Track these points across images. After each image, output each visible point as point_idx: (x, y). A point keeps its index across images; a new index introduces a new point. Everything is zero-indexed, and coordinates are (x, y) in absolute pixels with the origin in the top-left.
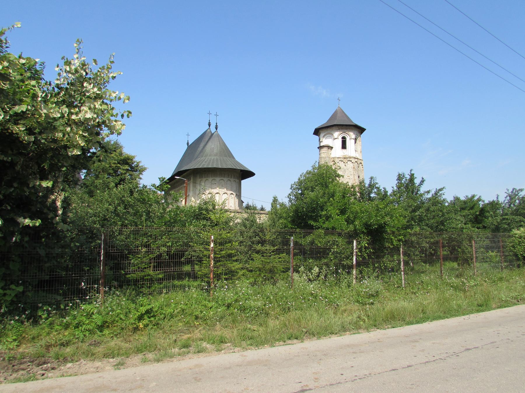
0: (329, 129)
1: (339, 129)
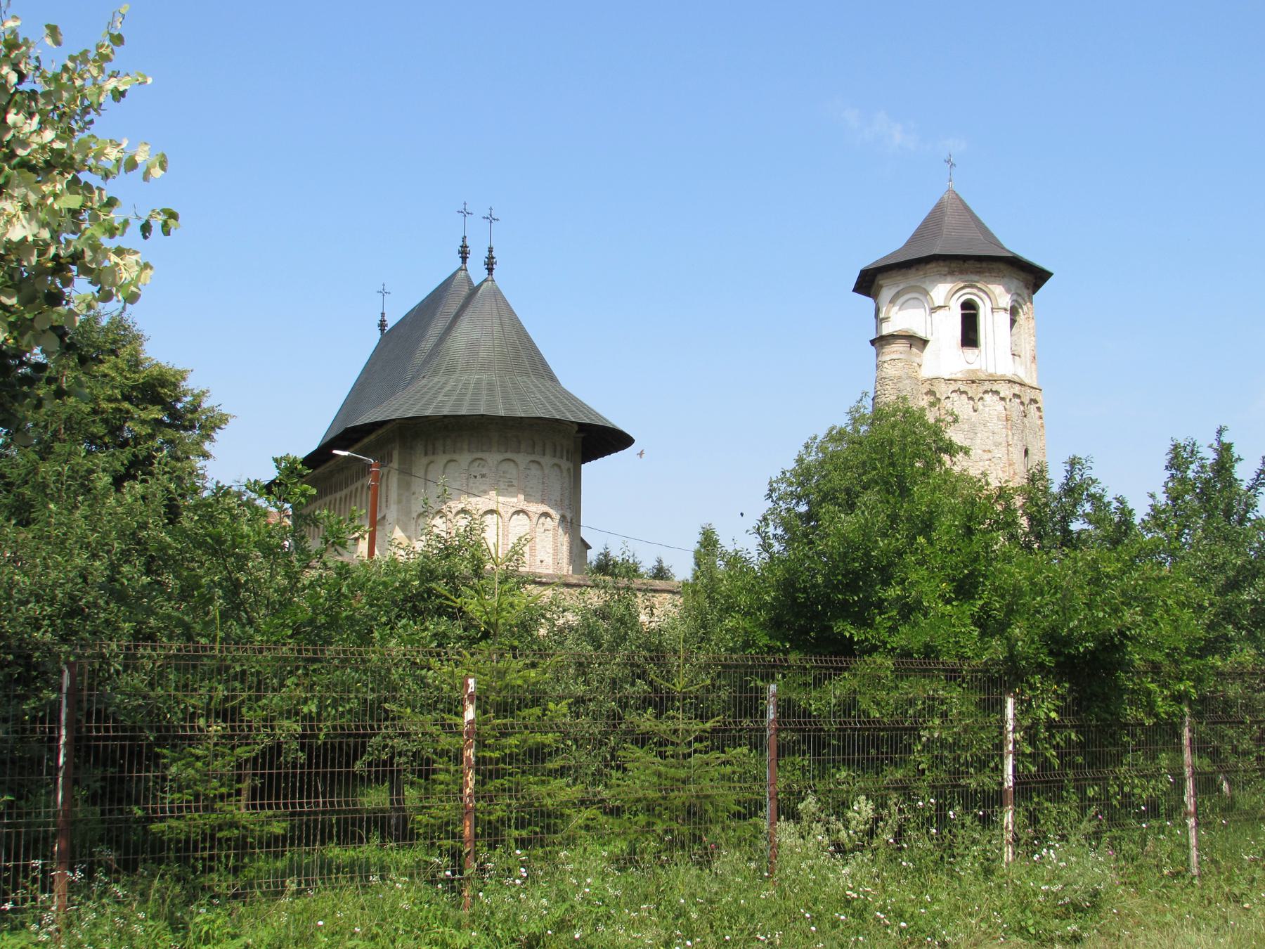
0: (913, 270)
1: (951, 273)
